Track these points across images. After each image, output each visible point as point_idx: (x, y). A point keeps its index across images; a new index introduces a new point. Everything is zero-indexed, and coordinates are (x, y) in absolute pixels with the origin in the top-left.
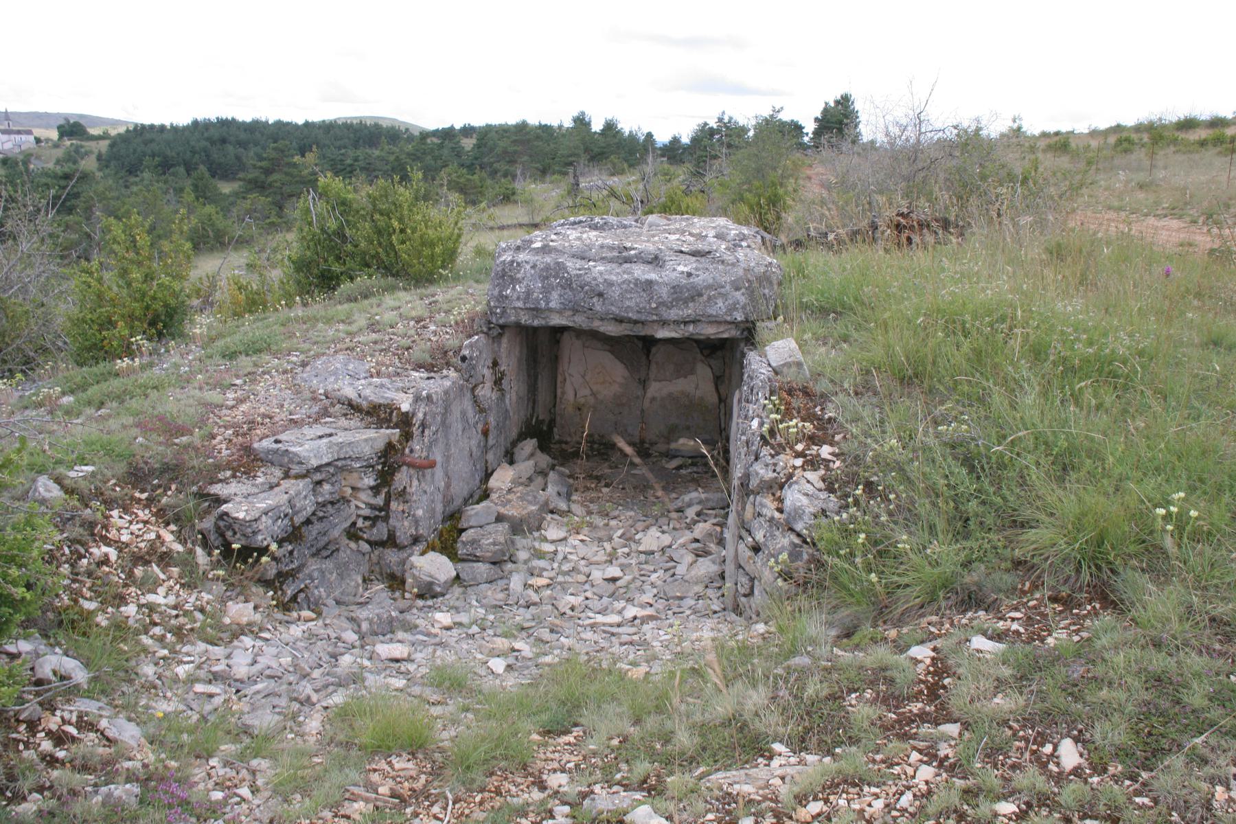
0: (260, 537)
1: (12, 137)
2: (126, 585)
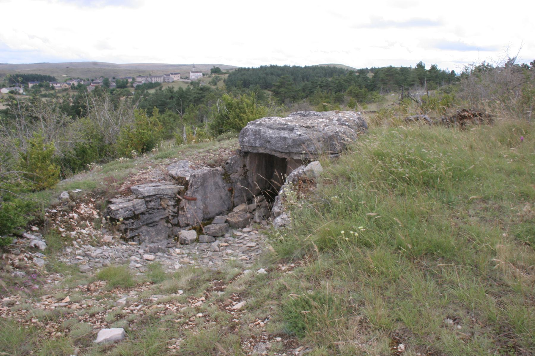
0: (118, 216)
1: (195, 74)
2: (76, 226)
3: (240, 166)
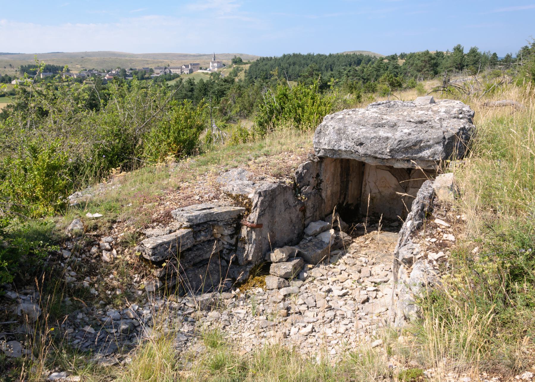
3: (312, 176)
